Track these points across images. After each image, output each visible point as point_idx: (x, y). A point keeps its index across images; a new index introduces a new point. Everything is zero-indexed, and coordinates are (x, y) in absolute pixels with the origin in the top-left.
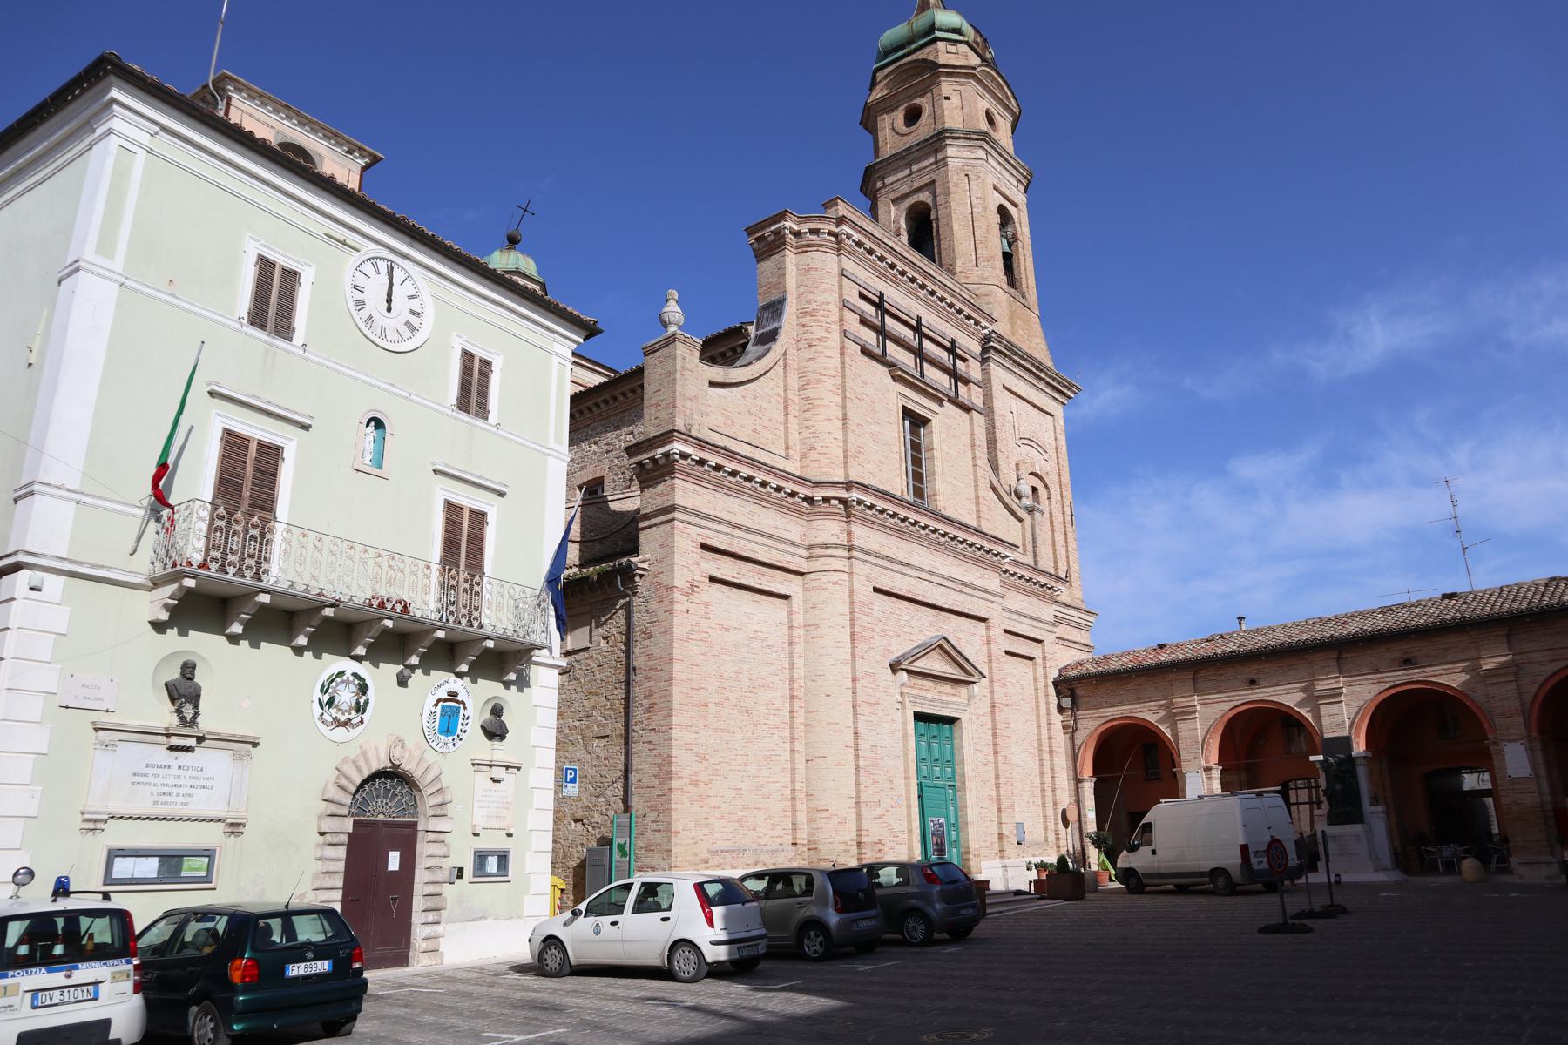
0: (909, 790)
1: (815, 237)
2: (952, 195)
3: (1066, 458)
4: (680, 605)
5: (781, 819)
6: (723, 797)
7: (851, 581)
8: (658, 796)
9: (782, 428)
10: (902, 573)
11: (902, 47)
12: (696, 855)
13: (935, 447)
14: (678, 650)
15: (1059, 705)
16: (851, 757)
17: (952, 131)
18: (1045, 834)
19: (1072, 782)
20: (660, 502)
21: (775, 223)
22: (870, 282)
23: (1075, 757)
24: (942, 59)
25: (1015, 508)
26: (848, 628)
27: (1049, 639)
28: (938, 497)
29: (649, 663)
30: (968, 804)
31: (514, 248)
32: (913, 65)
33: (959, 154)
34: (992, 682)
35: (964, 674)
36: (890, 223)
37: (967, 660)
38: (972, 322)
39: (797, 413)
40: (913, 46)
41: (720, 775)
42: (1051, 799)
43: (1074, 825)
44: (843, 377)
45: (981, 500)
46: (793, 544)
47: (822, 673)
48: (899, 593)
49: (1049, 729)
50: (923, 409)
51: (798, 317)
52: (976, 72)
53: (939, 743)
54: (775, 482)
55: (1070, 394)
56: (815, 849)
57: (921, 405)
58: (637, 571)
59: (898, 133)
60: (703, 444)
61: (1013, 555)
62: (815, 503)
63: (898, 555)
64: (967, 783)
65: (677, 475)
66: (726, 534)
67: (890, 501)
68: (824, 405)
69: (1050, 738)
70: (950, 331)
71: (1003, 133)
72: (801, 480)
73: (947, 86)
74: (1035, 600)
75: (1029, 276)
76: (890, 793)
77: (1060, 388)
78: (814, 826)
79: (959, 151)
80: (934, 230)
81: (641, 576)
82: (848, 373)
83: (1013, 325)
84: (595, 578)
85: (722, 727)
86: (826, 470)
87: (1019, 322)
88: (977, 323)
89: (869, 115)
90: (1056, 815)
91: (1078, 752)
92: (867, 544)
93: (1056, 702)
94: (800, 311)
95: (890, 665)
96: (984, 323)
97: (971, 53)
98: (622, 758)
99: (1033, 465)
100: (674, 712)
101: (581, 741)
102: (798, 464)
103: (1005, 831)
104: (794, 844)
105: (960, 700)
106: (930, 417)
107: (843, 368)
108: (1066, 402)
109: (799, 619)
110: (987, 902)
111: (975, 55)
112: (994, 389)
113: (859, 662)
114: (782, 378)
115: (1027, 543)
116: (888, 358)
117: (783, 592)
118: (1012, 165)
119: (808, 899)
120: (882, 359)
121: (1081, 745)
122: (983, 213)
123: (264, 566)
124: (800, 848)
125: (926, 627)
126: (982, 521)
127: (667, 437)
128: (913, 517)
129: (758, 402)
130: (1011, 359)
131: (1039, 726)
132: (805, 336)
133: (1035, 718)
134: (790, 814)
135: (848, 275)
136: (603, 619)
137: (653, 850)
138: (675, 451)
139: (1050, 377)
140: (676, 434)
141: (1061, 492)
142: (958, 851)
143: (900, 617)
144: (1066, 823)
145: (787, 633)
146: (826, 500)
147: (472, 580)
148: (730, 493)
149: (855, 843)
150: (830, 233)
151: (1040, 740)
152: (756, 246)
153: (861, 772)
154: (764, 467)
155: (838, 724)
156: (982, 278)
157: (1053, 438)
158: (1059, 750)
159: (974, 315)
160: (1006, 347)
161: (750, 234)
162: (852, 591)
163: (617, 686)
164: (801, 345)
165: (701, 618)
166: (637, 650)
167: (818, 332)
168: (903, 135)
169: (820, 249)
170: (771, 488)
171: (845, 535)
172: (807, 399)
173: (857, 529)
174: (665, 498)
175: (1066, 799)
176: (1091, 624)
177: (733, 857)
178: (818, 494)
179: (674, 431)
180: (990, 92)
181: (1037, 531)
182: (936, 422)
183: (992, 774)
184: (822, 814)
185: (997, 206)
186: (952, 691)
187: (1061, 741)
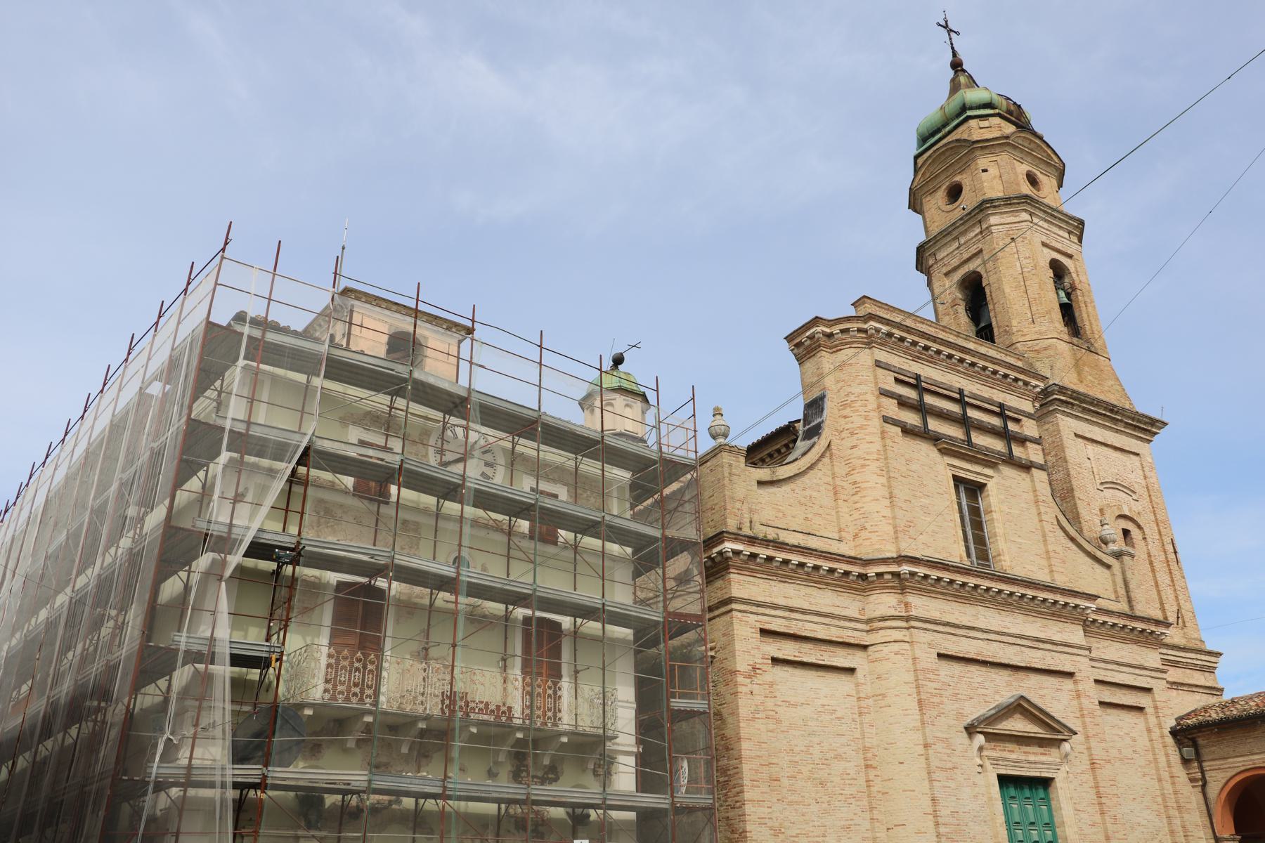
10: (966, 637)
11: (938, 131)
14: (745, 729)
15: (1183, 759)
16: (931, 824)
17: (991, 201)
22: (906, 367)
24: (976, 136)
25: (1099, 554)
26: (915, 695)
27: (1158, 686)
33: (1002, 221)
34: (1087, 737)
38: (1021, 383)
40: (947, 129)
44: (886, 459)
45: (1052, 554)
46: (851, 620)
48: (967, 656)
49: (1173, 783)
57: (972, 471)
60: (752, 540)
65: (731, 570)
66: (783, 618)
72: (852, 560)
74: (1135, 647)
83: (1079, 374)
87: (1086, 369)
88: (1026, 384)
89: (915, 199)
92: (926, 613)
96: (1034, 382)
97: (1004, 123)
99: (1120, 507)
107: (885, 451)
109: (867, 690)
111: (1009, 124)
112: (1064, 439)
115: (1119, 589)
117: (847, 665)
118: (1060, 219)
122: (1034, 272)
125: (1003, 689)
129: (808, 493)
132: (847, 426)
139: (1129, 417)
140: (725, 535)
146: (879, 575)
152: (796, 351)
155: (914, 791)
156: (1040, 333)
157: (1142, 477)
158: (1188, 806)
162: (914, 659)
165: (765, 697)
167: (858, 421)
169: (853, 346)
171: (903, 606)
172: (855, 483)
174: (724, 591)
178: (871, 571)
181: (1129, 575)
182: (991, 486)
186: (1041, 750)
187: (1192, 796)
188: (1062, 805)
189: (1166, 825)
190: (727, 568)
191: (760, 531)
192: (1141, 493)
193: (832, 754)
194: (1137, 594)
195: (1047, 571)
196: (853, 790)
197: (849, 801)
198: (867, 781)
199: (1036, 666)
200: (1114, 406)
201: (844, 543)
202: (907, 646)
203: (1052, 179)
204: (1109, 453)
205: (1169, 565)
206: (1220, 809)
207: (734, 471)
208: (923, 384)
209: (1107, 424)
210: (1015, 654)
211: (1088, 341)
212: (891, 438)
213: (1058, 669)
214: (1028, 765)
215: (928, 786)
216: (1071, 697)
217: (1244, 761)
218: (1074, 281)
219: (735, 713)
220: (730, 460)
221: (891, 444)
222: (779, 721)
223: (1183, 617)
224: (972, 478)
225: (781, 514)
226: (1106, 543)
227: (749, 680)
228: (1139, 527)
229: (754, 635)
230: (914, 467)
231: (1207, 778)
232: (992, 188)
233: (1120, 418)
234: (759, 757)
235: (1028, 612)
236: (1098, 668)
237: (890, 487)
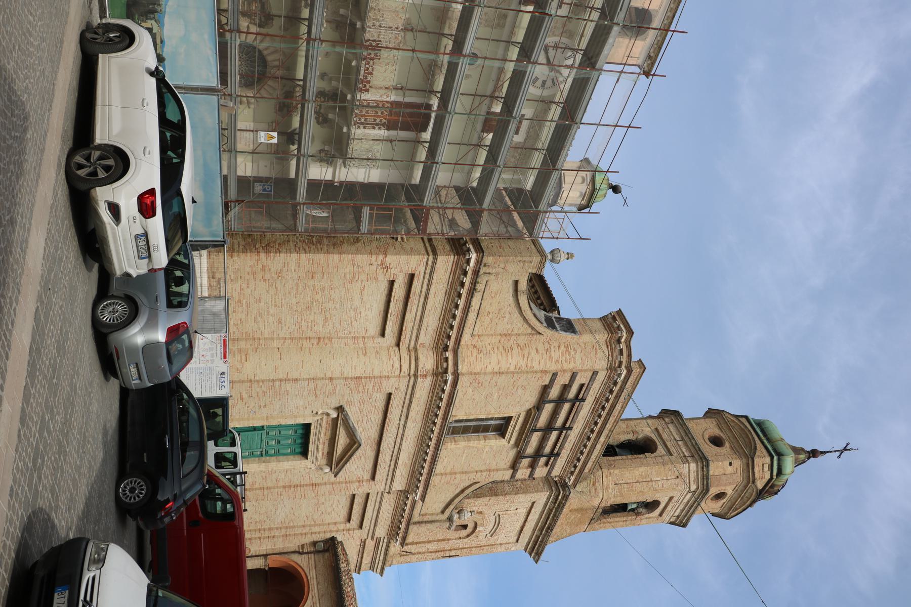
5: (241, 330)
6: (255, 290)
11: (765, 435)
14: (347, 258)
15: (317, 542)
16: (281, 376)
17: (708, 466)
21: (625, 327)
22: (591, 392)
25: (452, 507)
26: (364, 375)
27: (363, 533)
33: (692, 472)
34: (333, 484)
36: (641, 427)
40: (765, 442)
44: (527, 372)
45: (453, 476)
46: (417, 337)
48: (389, 412)
49: (301, 534)
53: (290, 445)
57: (514, 430)
60: (476, 273)
63: (413, 411)
64: (264, 464)
65: (456, 257)
66: (421, 291)
72: (458, 342)
78: (236, 352)
82: (530, 375)
83: (576, 510)
85: (300, 289)
87: (579, 515)
88: (572, 473)
89: (715, 413)
95: (341, 406)
96: (573, 478)
97: (765, 481)
99: (482, 525)
100: (308, 255)
106: (506, 438)
107: (533, 372)
111: (763, 485)
112: (531, 495)
118: (689, 511)
122: (652, 489)
123: (362, 127)
125: (366, 432)
127: (479, 249)
129: (507, 316)
131: (303, 526)
140: (481, 254)
141: (464, 548)
143: (373, 413)
146: (446, 359)
147: (381, 125)
152: (610, 316)
155: (302, 368)
156: (607, 488)
157: (501, 542)
158: (287, 541)
160: (560, 502)
162: (388, 377)
164: (547, 344)
167: (556, 355)
169: (610, 357)
171: (425, 373)
172: (512, 349)
174: (442, 250)
178: (449, 354)
179: (484, 253)
181: (437, 524)
182: (503, 442)
183: (269, 484)
184: (244, 358)
185: (658, 499)
188: (290, 462)
190: (458, 254)
191: (482, 280)
193: (328, 316)
194: (423, 528)
195: (443, 471)
196: (304, 328)
197: (297, 325)
200: (552, 530)
202: (397, 373)
205: (441, 551)
209: (540, 524)
210: (388, 444)
211: (599, 519)
215: (305, 377)
219: (358, 252)
222: (351, 282)
225: (493, 295)
226: (458, 513)
228: (468, 536)
229: (410, 269)
230: (520, 391)
232: (717, 467)
233: (543, 533)
234: (328, 266)
236: (377, 497)
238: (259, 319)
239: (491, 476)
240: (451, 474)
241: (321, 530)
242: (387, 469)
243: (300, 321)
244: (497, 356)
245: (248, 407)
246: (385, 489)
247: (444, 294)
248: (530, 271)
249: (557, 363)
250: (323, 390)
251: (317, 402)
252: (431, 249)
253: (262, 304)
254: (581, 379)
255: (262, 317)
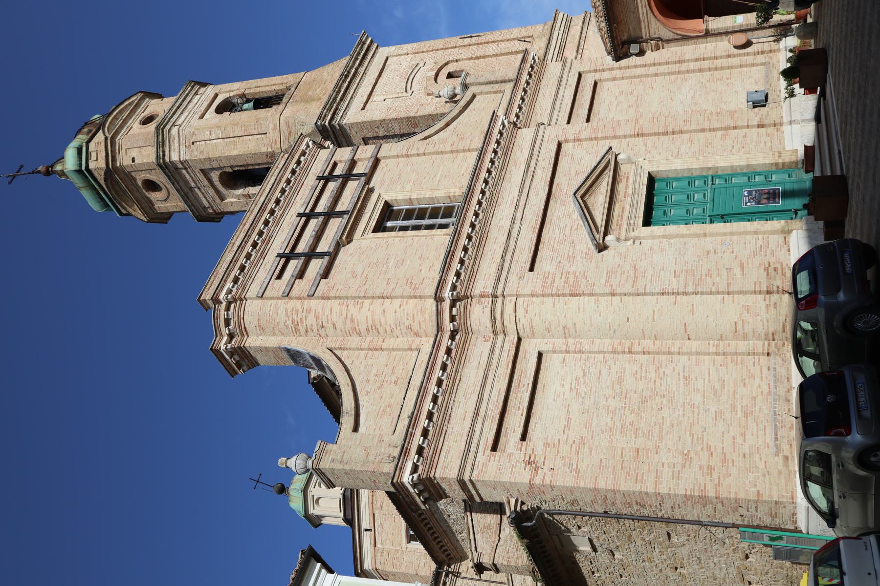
0: (717, 234)
1: (232, 321)
2: (211, 156)
3: (422, 43)
4: (546, 478)
5: (744, 368)
6: (723, 433)
7: (524, 296)
8: (723, 506)
9: (394, 353)
12: (780, 473)
13: (408, 197)
14: (586, 483)
15: (638, 55)
16: (685, 298)
17: (158, 157)
18: (757, 65)
19: (708, 39)
20: (457, 488)
21: (223, 356)
22: (268, 267)
23: (686, 38)
24: (102, 164)
25: (462, 103)
26: (566, 298)
27: (577, 67)
28: (451, 195)
29: (600, 502)
30: (729, 164)
31: (288, 488)
32: (111, 187)
33: (177, 150)
34: (615, 137)
35: (608, 170)
36: (240, 202)
37: (595, 168)
38: (302, 159)
39: (381, 339)
41: (703, 435)
42: (724, 60)
43: (753, 36)
44: (347, 298)
45: (454, 148)
46: (492, 351)
47: (608, 325)
49: (660, 64)
50: (376, 211)
51: (300, 336)
52: (109, 136)
53: (673, 193)
54: (438, 373)
55: (368, 42)
56: (773, 334)
57: (372, 213)
58: (518, 509)
59: (168, 197)
60: (404, 451)
61: (501, 113)
62: (456, 329)
64: (710, 166)
66: (483, 423)
67: (453, 255)
68: (372, 316)
69: (667, 63)
70: (310, 181)
71: (157, 107)
72: (436, 345)
73: (124, 160)
74: (543, 82)
75: (272, 83)
76: (719, 255)
77: (363, 52)
78: (751, 335)
79: (174, 150)
80: (241, 169)
81: (523, 503)
83: (313, 100)
84: (526, 541)
86: (427, 316)
87: (310, 93)
88: (303, 154)
90: (739, 55)
91: (681, 35)
93: (634, 57)
94: (295, 334)
95: (600, 251)
96: (303, 147)
97: (96, 140)
98: (687, 526)
99: (428, 79)
101: (673, 549)
102: (424, 339)
103: (755, 122)
104: (768, 354)
105: (632, 172)
106: (383, 202)
107: (340, 298)
108: (376, 45)
109: (559, 343)
110: (829, 174)
112: (365, 119)
113: (597, 290)
114: (352, 352)
116: (331, 250)
118: (183, 101)
119: (833, 459)
120: (333, 256)
121: (674, 33)
124: (773, 349)
126: (472, 147)
128: (470, 217)
130: (339, 103)
131: (657, 75)
132: (315, 331)
133: (649, 79)
134: (739, 357)
135: (262, 291)
136: (563, 528)
137: (776, 513)
138: (410, 480)
139: (354, 63)
140: (395, 481)
142: (775, 173)
144: (748, 44)
145: (572, 355)
146: (453, 319)
148: (447, 418)
149: (768, 296)
150: (228, 309)
151: (669, 74)
152: (245, 368)
153: (699, 289)
154: (424, 384)
155: (654, 311)
156: (275, 129)
157: (406, 56)
158: (679, 54)
159: (296, 157)
161: (236, 373)
162: (532, 295)
163: (621, 523)
164: (323, 334)
166: (589, 510)
168: (169, 193)
169: (242, 316)
170: (443, 375)
171: (483, 299)
172: (368, 330)
173: (477, 291)
174: (453, 484)
175: (724, 45)
176: (566, 16)
177: (782, 427)
178: (448, 326)
180: (125, 122)
181: (482, 80)
182: (387, 197)
184: (740, 327)
186: (624, 180)
188: (673, 168)
189: (694, 74)
190: (430, 480)
191: (399, 438)
192: (420, 59)
193: (617, 386)
194: (499, 76)
195: (468, 154)
196: (652, 369)
197: (661, 375)
198: (644, 354)
199: (550, 176)
200: (342, 74)
201: (422, 347)
202: (520, 300)
203: (151, 103)
204: (382, 83)
205: (481, 44)
206: (659, 77)
207: (339, 458)
208: (286, 252)
211: (289, 89)
212: (329, 290)
213: (554, 156)
214: (636, 195)
215: (650, 297)
216: (580, 147)
217: (642, 6)
218: (236, 95)
219: (571, 490)
220: (328, 460)
221: (334, 291)
222: (582, 440)
223: (524, 37)
224: (378, 215)
225: (388, 409)
226: (455, 95)
227: (540, 470)
228: (446, 64)
229: (497, 458)
230: (359, 270)
231: (656, 36)
232: (149, 156)
234: (614, 470)
235: (501, 178)
236: (558, 116)
237: (373, 298)
238: (717, 386)
239: (405, 149)
240: (458, 151)
241: (634, 69)
242: (540, 158)
243: (658, 380)
244: (386, 321)
245: (733, 252)
246: (545, 129)
247: (452, 416)
248: (335, 447)
249: (309, 309)
250: (624, 277)
251: (634, 259)
252: (467, 487)
253: (713, 410)
254: (280, 286)
255: (713, 388)
